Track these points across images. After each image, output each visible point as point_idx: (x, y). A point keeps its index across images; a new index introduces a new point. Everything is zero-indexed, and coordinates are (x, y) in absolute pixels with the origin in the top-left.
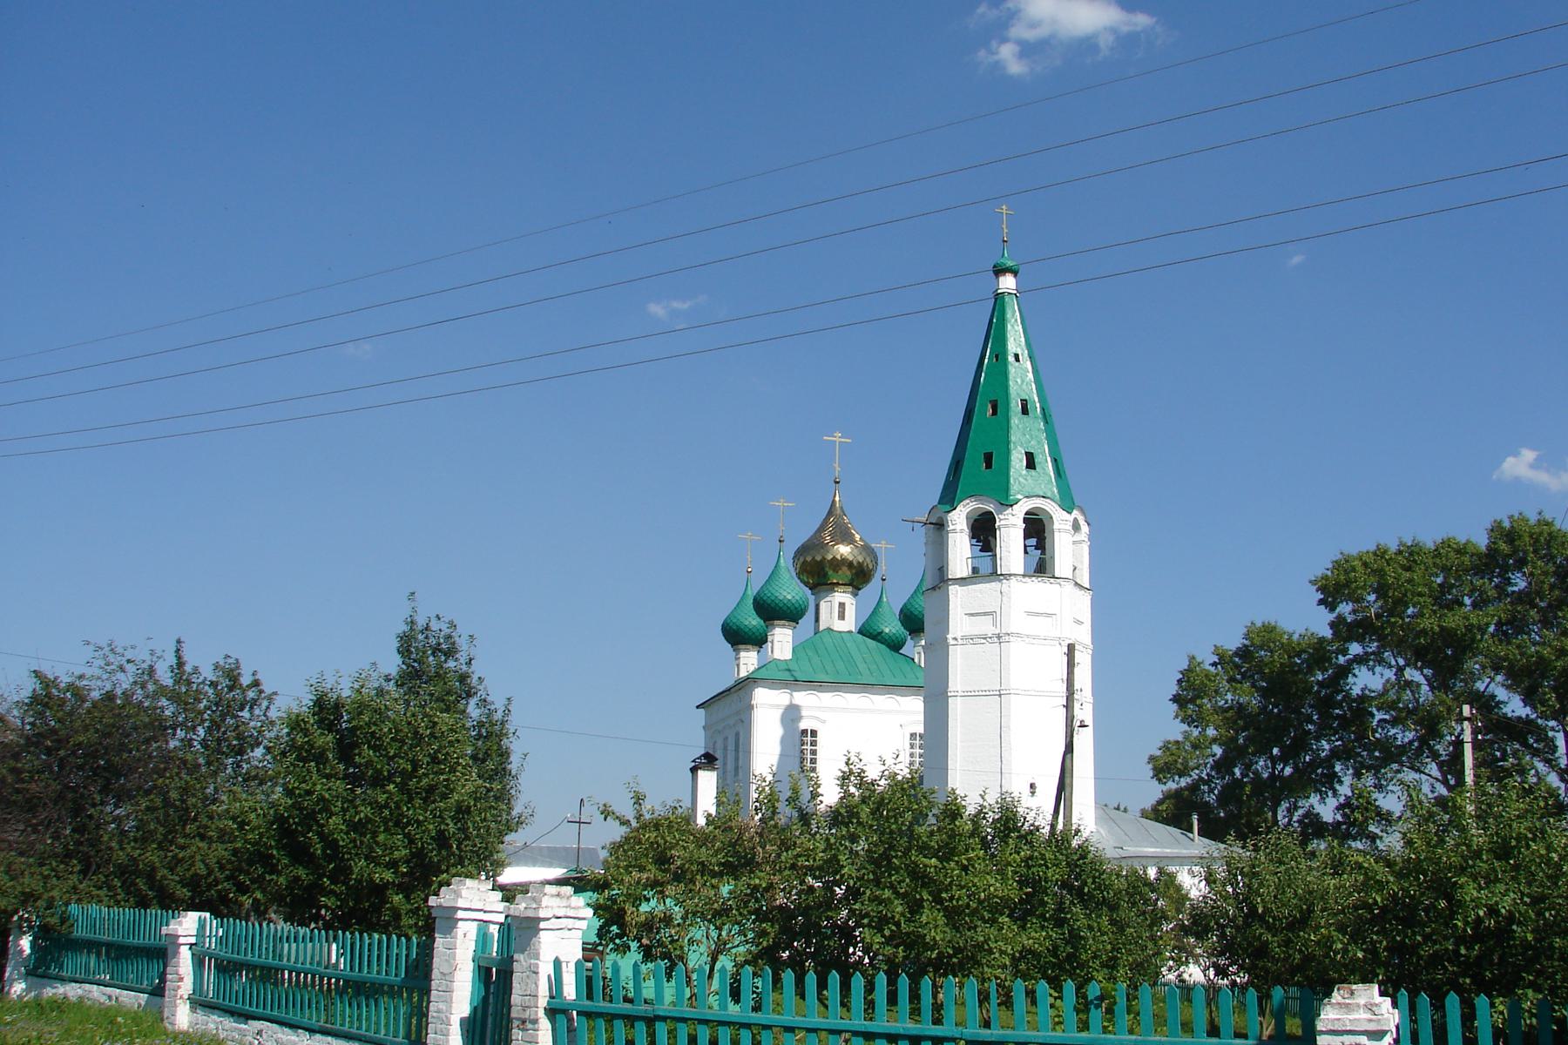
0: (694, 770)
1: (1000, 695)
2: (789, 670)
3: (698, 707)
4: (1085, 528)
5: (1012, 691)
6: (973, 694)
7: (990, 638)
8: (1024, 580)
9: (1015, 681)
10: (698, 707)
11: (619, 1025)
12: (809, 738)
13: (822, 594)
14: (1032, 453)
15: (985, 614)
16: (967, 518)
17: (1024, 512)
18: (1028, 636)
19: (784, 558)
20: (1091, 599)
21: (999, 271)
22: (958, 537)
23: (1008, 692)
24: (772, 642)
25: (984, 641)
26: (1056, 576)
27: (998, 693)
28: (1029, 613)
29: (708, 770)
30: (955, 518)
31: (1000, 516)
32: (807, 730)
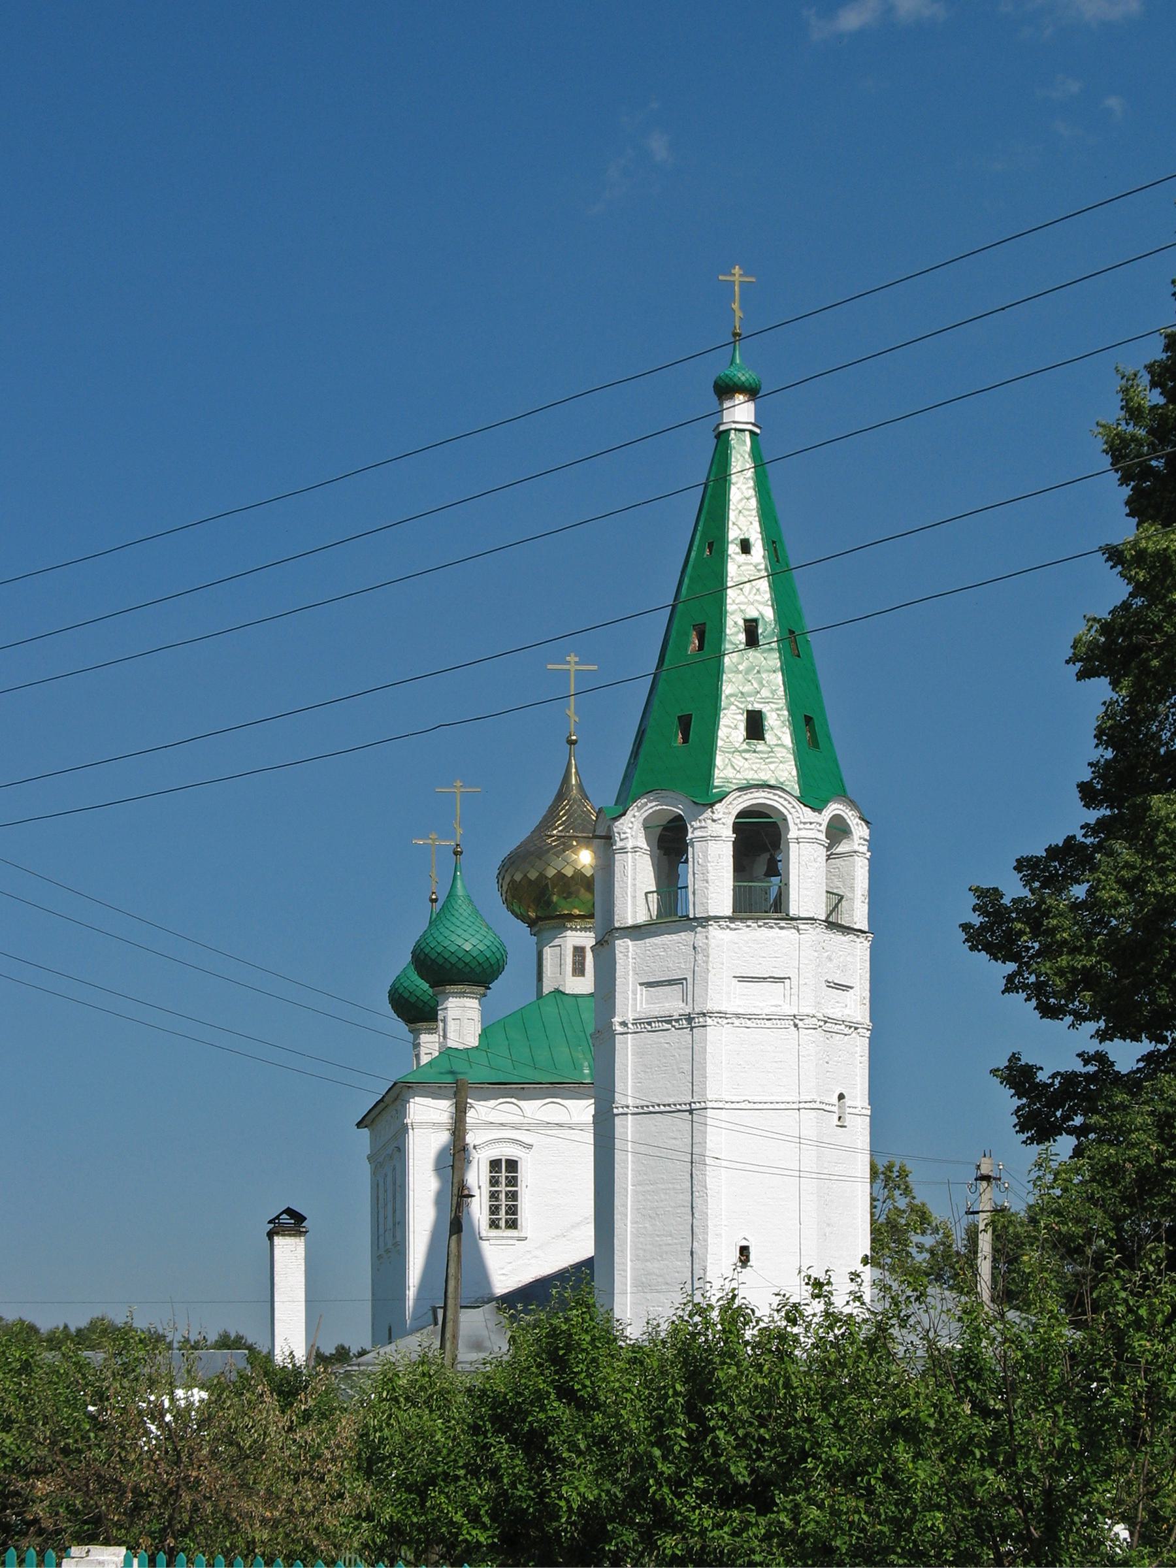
1: (691, 1112)
2: (452, 1073)
3: (359, 1125)
4: (860, 831)
5: (709, 1105)
7: (677, 1021)
8: (732, 926)
10: (359, 1125)
12: (504, 1174)
14: (759, 713)
15: (670, 983)
16: (645, 828)
17: (735, 813)
18: (738, 1016)
19: (462, 881)
20: (871, 947)
21: (725, 390)
22: (630, 860)
24: (444, 1021)
27: (688, 1108)
28: (743, 979)
29: (290, 1235)
30: (625, 829)
31: (693, 823)
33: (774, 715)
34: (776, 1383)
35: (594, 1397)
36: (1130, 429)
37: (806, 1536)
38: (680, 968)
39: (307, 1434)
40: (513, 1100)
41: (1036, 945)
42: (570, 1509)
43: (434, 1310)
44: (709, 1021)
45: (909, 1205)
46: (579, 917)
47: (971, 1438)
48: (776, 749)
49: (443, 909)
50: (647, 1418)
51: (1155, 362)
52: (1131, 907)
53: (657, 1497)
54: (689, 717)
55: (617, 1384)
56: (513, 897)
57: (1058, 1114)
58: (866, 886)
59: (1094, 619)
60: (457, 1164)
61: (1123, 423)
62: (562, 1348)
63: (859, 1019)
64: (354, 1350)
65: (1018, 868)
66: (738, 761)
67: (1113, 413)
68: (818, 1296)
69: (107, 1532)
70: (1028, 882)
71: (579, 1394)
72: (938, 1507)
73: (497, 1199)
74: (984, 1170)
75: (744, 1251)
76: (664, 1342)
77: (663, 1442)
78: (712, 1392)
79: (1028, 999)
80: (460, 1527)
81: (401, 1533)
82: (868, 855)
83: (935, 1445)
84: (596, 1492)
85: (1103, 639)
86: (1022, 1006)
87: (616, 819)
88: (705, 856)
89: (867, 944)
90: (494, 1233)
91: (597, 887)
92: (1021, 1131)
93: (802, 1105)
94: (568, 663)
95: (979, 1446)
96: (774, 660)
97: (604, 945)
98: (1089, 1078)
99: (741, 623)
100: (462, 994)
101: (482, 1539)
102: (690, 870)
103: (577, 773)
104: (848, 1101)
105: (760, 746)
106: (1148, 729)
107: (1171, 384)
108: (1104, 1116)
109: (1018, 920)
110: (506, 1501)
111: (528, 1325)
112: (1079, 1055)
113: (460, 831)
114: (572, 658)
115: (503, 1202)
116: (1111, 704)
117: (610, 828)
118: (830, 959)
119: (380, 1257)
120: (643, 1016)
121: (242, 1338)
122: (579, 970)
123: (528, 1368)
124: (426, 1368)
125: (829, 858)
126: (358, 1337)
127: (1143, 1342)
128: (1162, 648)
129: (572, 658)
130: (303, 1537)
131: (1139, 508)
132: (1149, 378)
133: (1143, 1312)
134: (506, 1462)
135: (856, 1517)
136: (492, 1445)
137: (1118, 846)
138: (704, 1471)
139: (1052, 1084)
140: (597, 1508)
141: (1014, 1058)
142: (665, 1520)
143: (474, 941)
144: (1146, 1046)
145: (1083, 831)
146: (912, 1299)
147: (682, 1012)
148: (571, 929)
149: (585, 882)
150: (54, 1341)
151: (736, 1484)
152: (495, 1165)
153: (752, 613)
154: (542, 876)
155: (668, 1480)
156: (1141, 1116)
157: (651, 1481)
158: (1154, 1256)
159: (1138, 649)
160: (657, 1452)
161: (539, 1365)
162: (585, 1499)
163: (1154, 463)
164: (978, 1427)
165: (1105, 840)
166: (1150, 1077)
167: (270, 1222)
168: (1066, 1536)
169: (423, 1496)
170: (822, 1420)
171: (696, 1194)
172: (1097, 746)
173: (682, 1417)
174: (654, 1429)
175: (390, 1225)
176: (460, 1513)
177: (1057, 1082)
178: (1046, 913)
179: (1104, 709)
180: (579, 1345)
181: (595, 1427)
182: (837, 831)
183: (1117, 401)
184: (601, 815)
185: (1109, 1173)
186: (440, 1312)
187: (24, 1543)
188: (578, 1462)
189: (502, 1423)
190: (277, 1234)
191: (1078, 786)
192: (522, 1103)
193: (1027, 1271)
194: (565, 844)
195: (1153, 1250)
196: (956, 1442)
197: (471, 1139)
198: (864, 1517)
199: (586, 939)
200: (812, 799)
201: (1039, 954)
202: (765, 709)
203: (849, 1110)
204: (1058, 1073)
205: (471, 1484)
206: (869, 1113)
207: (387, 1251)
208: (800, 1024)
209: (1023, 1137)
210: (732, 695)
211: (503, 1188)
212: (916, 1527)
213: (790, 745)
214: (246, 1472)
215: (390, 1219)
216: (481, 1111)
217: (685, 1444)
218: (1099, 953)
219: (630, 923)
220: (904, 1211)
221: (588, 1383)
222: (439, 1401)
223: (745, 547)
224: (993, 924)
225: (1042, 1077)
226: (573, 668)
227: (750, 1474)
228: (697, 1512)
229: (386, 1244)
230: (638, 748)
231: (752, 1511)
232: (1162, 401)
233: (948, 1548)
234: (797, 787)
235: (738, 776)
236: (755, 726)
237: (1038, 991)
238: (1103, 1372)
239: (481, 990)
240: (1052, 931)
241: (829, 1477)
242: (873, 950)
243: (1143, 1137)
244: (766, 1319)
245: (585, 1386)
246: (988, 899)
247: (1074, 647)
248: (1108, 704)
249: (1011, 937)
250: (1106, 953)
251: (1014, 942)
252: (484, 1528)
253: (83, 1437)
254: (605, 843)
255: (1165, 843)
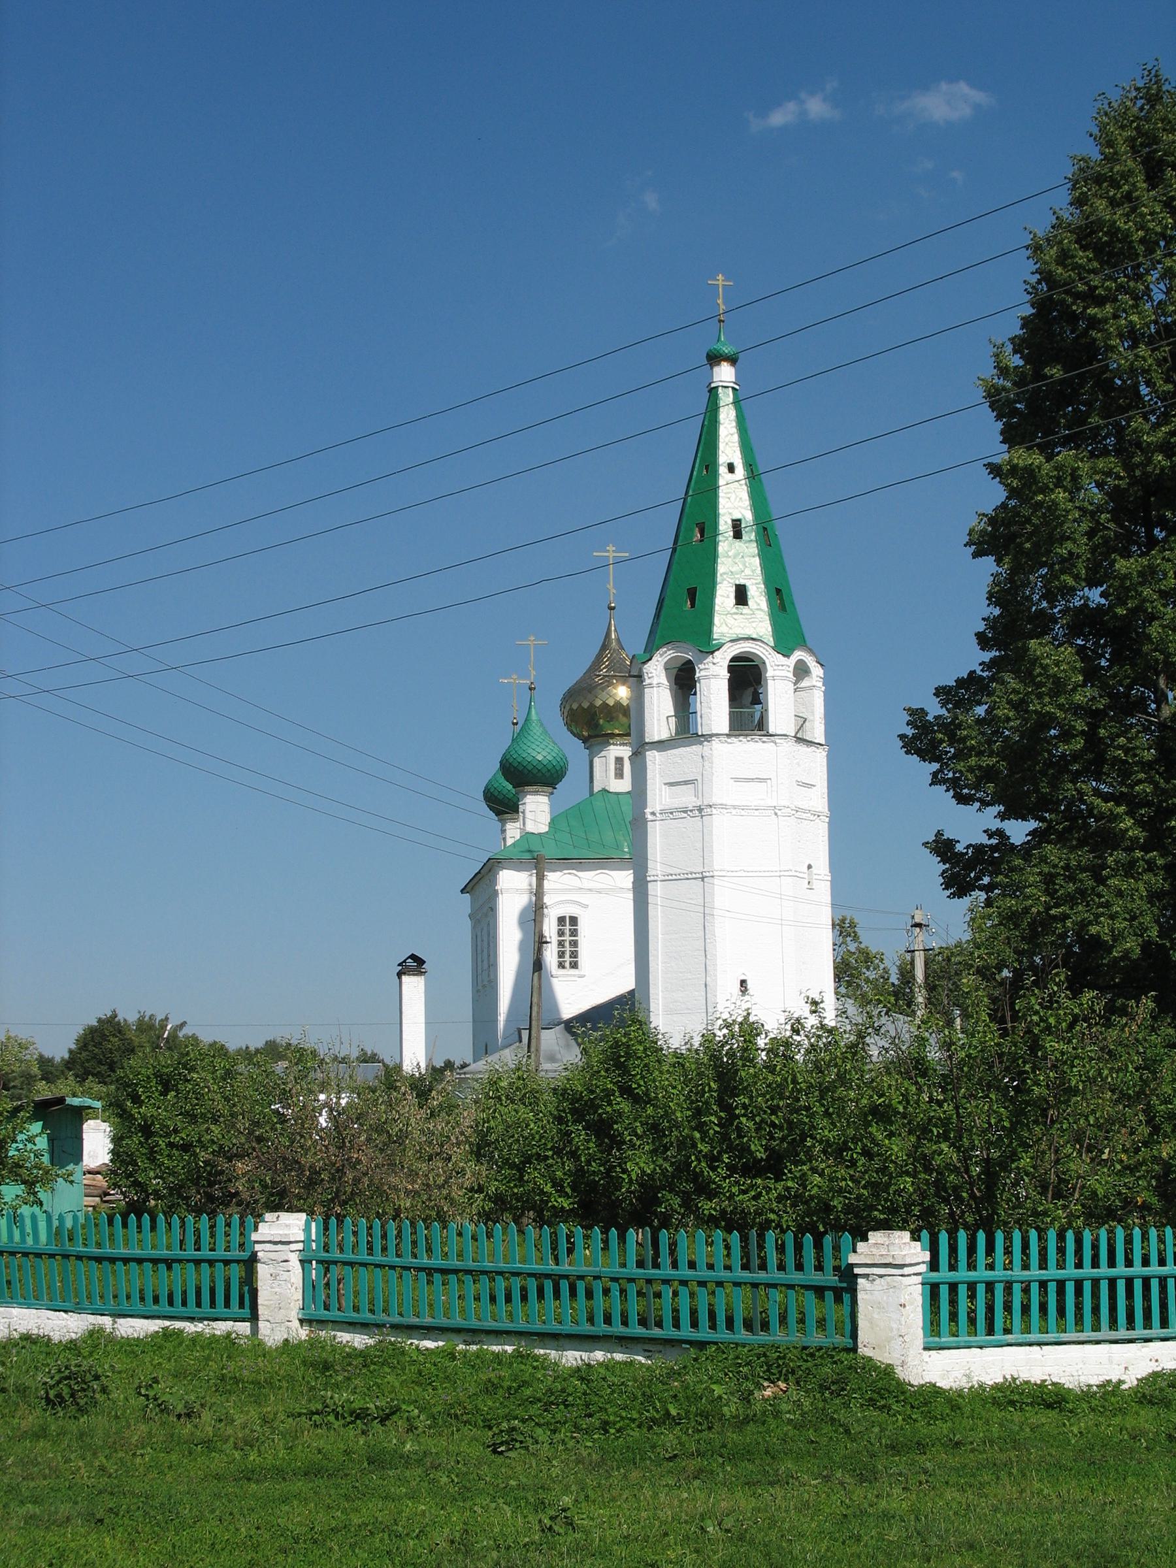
0: (400, 975)
1: (703, 879)
2: (530, 851)
3: (462, 891)
4: (817, 671)
5: (716, 873)
6: (674, 877)
7: (691, 811)
8: (729, 740)
9: (722, 859)
10: (462, 891)
11: (205, 1266)
12: (568, 927)
13: (595, 749)
14: (744, 586)
15: (686, 783)
16: (666, 669)
17: (729, 658)
18: (735, 807)
21: (714, 359)
23: (711, 874)
24: (523, 813)
25: (685, 815)
26: (771, 731)
28: (737, 780)
29: (414, 975)
32: (565, 917)
33: (754, 588)
34: (786, 1079)
35: (647, 1094)
36: (1001, 381)
37: (812, 1197)
38: (692, 772)
39: (439, 1125)
40: (574, 871)
41: (952, 750)
42: (631, 1180)
43: (519, 1031)
44: (714, 811)
45: (858, 948)
46: (619, 735)
47: (930, 1119)
48: (756, 612)
49: (522, 731)
50: (688, 1109)
51: (1016, 336)
52: (1018, 722)
53: (697, 1170)
54: (695, 589)
55: (667, 1083)
56: (572, 721)
57: (972, 875)
58: (822, 711)
59: (983, 515)
60: (538, 919)
61: (996, 377)
62: (623, 1057)
63: (820, 809)
64: (457, 1064)
65: (937, 695)
66: (730, 620)
67: (989, 371)
68: (815, 1012)
69: (289, 1201)
70: (944, 705)
71: (636, 1091)
72: (907, 1173)
73: (563, 946)
74: (917, 920)
75: (743, 983)
76: (697, 1050)
77: (700, 1127)
78: (735, 1088)
79: (947, 790)
80: (549, 1195)
81: (504, 1202)
82: (823, 688)
83: (904, 1125)
84: (652, 1167)
85: (990, 529)
86: (943, 796)
87: (645, 663)
88: (709, 690)
89: (825, 754)
90: (562, 972)
91: (633, 713)
92: (946, 888)
93: (782, 873)
94: (608, 551)
95: (936, 1126)
96: (753, 549)
97: (638, 755)
98: (993, 848)
99: (730, 522)
100: (536, 793)
101: (565, 1205)
102: (698, 700)
103: (615, 630)
104: (814, 870)
105: (744, 609)
106: (1024, 593)
107: (1026, 351)
108: (1006, 876)
109: (940, 732)
110: (583, 1176)
111: (596, 1039)
112: (985, 831)
113: (533, 673)
114: (611, 548)
115: (568, 949)
116: (997, 575)
117: (641, 670)
118: (798, 764)
119: (478, 991)
120: (667, 807)
121: (376, 1055)
122: (619, 774)
123: (600, 1072)
124: (520, 1073)
125: (795, 691)
126: (461, 1050)
127: (1053, 1044)
128: (1032, 534)
129: (611, 548)
130: (436, 1205)
131: (1010, 437)
132: (1012, 346)
133: (1052, 1020)
134: (583, 1145)
135: (844, 1183)
136: (572, 1132)
137: (1008, 677)
138: (731, 1148)
139: (967, 853)
140: (653, 1180)
141: (939, 834)
142: (706, 1190)
143: (544, 753)
144: (1033, 824)
145: (981, 667)
146: (883, 1014)
147: (694, 804)
148: (614, 744)
149: (621, 710)
150: (248, 1055)
151: (755, 1158)
152: (561, 920)
153: (737, 516)
154: (592, 705)
155: (705, 1156)
156: (1032, 875)
157: (693, 1158)
158: (1057, 980)
159: (1014, 536)
160: (697, 1135)
161: (607, 1070)
162: (643, 1172)
163: (1018, 406)
164: (935, 1110)
165: (998, 672)
166: (1038, 846)
167: (399, 965)
168: (1001, 1195)
169: (521, 1170)
170: (818, 1109)
171: (708, 941)
172: (988, 605)
173: (715, 1107)
174: (694, 1116)
175: (486, 966)
176: (549, 1185)
177: (970, 851)
178: (959, 726)
179: (992, 578)
180: (636, 1054)
181: (648, 1117)
182: (801, 671)
183: (991, 362)
184: (635, 661)
185: (1011, 918)
186: (525, 1034)
187: (229, 1211)
188: (638, 1143)
189: (579, 1115)
190: (405, 974)
191: (976, 635)
192: (580, 874)
193: (966, 990)
194: (608, 682)
195: (1057, 974)
196: (918, 1123)
197: (547, 900)
198: (849, 1183)
199: (625, 752)
200: (783, 647)
201: (954, 756)
202: (748, 583)
203: (815, 877)
204: (970, 845)
205: (557, 1162)
206: (829, 878)
207: (484, 986)
208: (779, 813)
209: (948, 893)
210: (724, 573)
211: (567, 938)
212: (892, 1189)
213: (766, 609)
214: (393, 1154)
215: (485, 962)
216: (555, 880)
217: (717, 1129)
218: (998, 755)
219: (656, 739)
220: (854, 953)
221: (642, 1083)
222: (530, 1098)
223: (731, 468)
224: (921, 735)
225: (960, 848)
226: (611, 555)
227: (766, 1151)
228: (727, 1181)
229: (482, 981)
230: (660, 611)
231: (771, 1179)
232: (1021, 363)
233: (915, 1206)
234: (771, 639)
235: (731, 632)
236: (741, 596)
237: (954, 785)
238: (1024, 1066)
239: (550, 789)
240: (963, 740)
241: (824, 1152)
242: (830, 759)
243: (1035, 891)
244: (775, 1032)
245: (640, 1086)
246: (917, 716)
247: (969, 534)
248: (995, 575)
249: (935, 744)
250: (1002, 755)
251: (936, 748)
252: (567, 1196)
253: (272, 1129)
254: (637, 679)
255: (1040, 674)
